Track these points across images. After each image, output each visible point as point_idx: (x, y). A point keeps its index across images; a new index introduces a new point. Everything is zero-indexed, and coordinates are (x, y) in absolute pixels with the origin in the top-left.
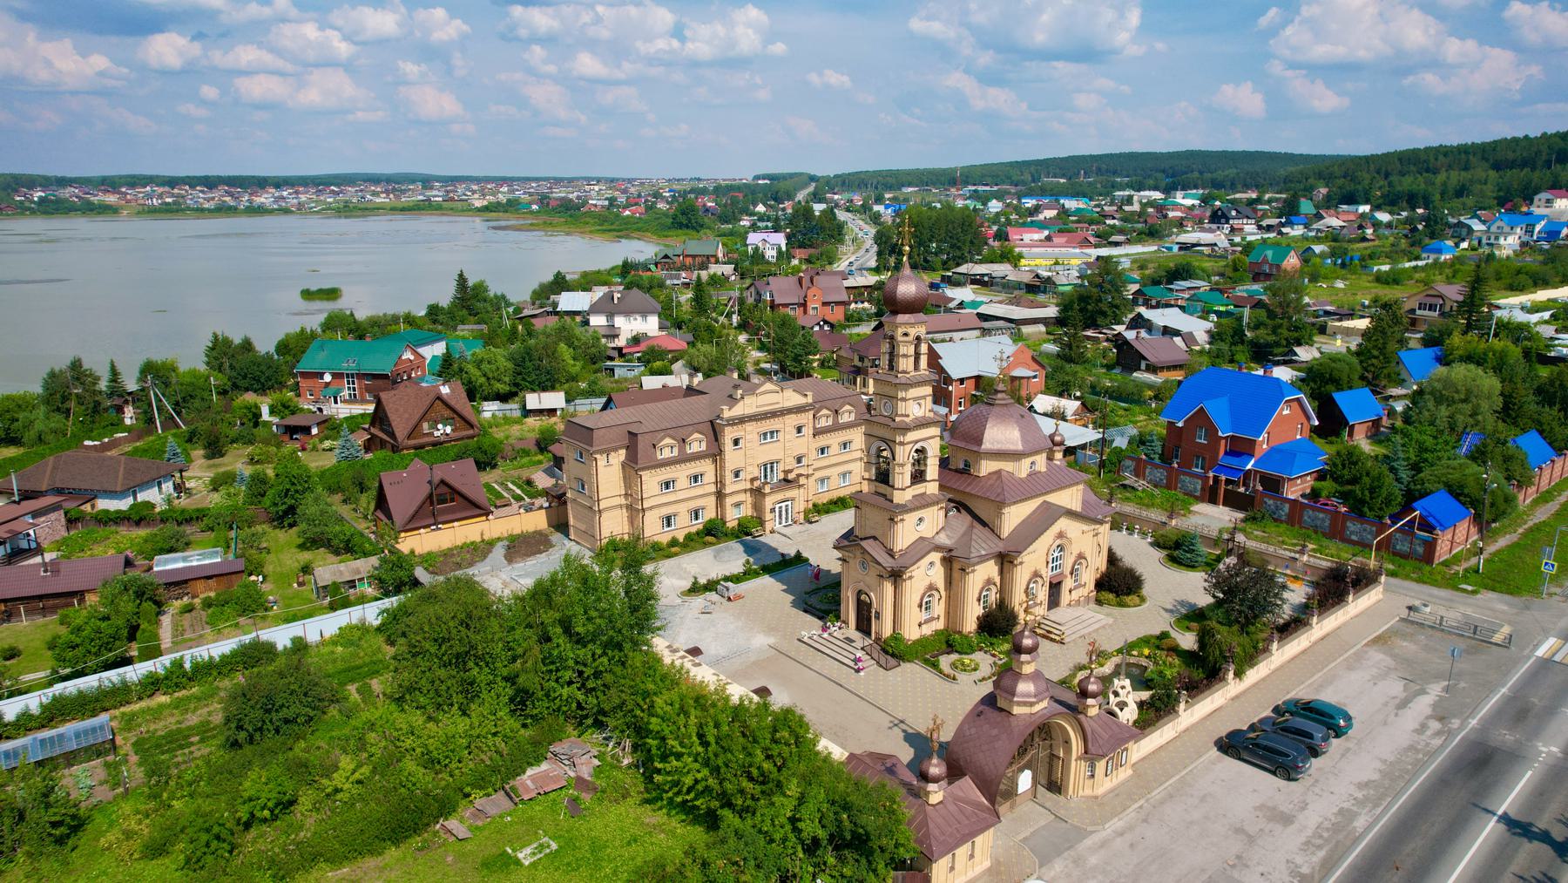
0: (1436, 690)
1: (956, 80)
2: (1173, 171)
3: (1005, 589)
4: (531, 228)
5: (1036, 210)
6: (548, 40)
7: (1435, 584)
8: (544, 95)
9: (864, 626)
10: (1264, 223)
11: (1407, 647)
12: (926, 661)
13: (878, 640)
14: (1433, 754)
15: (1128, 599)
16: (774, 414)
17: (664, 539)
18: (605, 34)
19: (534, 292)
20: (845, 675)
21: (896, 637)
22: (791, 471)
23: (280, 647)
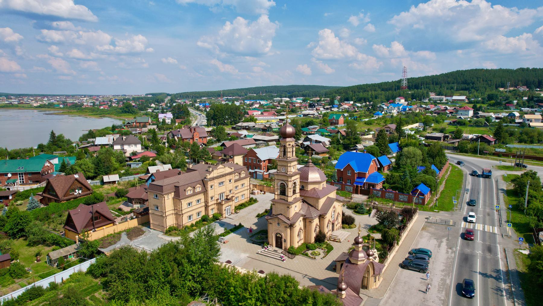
0: (444, 240)
1: (215, 62)
2: (292, 91)
3: (321, 226)
4: (63, 114)
5: (252, 105)
6: (59, 43)
7: (427, 211)
8: (57, 64)
9: (279, 244)
10: (326, 107)
11: (432, 229)
12: (303, 254)
13: (285, 249)
14: (454, 258)
15: (352, 226)
16: (223, 176)
17: (189, 224)
18: (82, 42)
19: (80, 138)
20: (279, 263)
21: (292, 247)
22: (228, 196)
23: (45, 287)
